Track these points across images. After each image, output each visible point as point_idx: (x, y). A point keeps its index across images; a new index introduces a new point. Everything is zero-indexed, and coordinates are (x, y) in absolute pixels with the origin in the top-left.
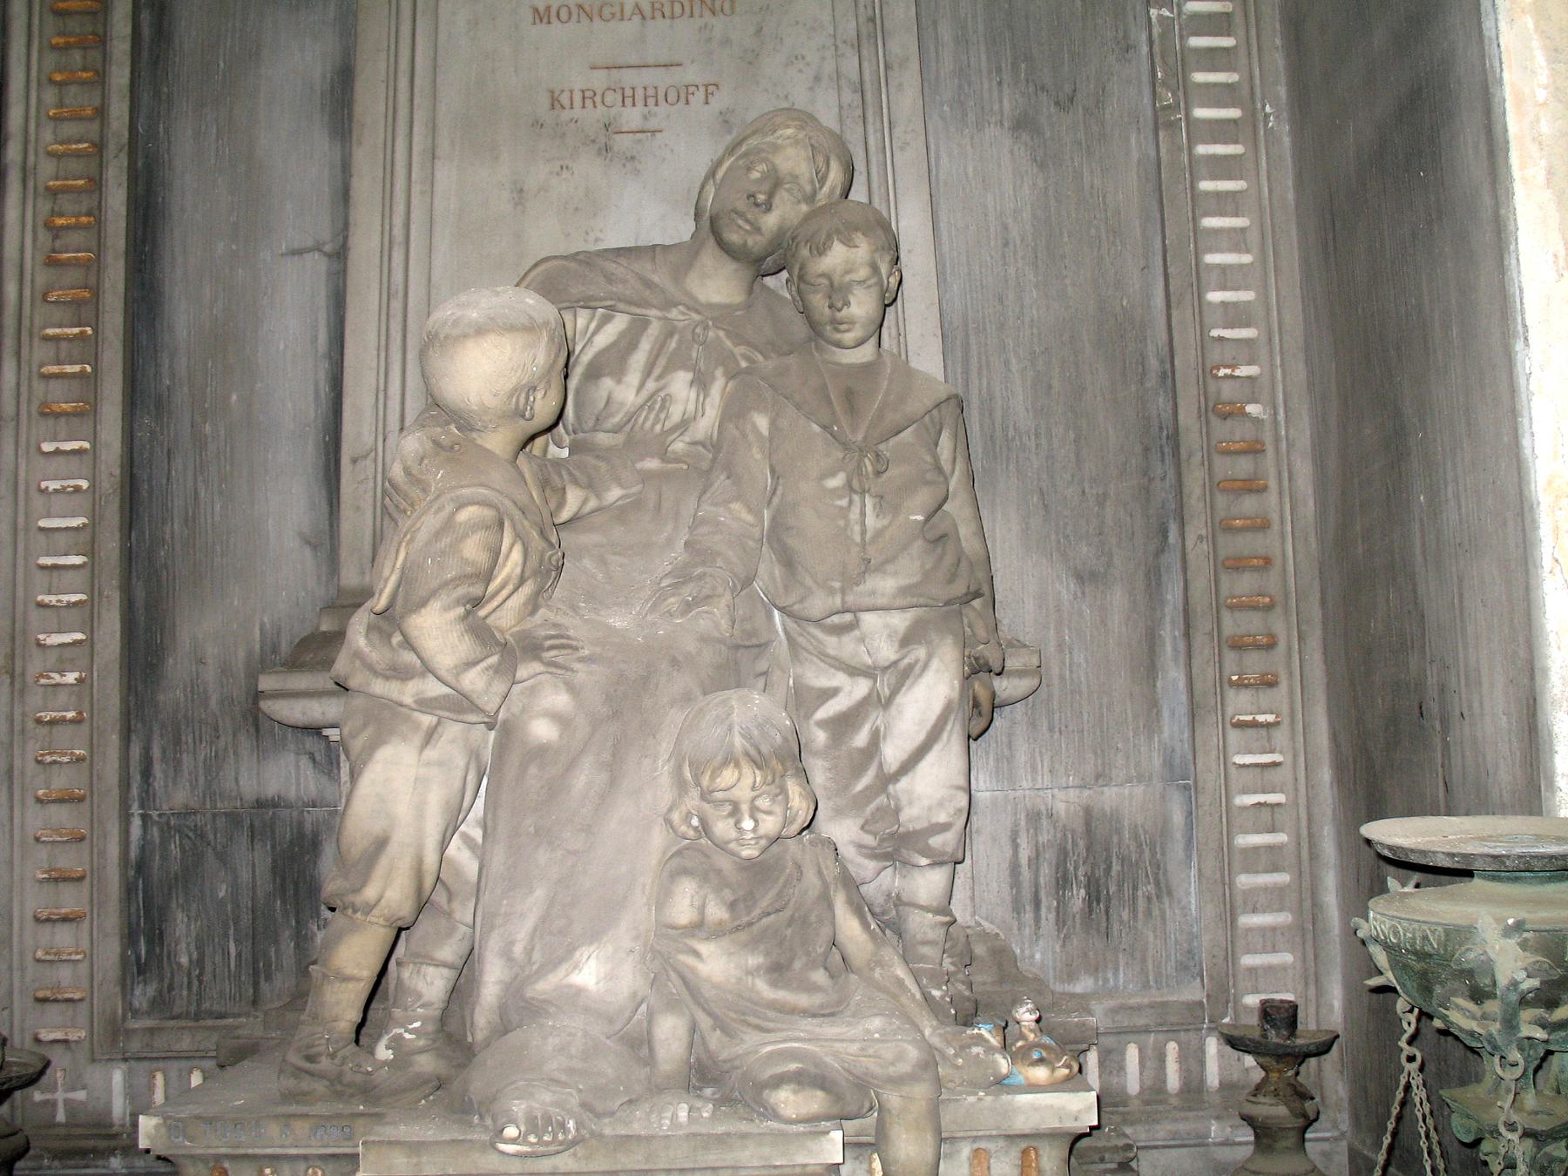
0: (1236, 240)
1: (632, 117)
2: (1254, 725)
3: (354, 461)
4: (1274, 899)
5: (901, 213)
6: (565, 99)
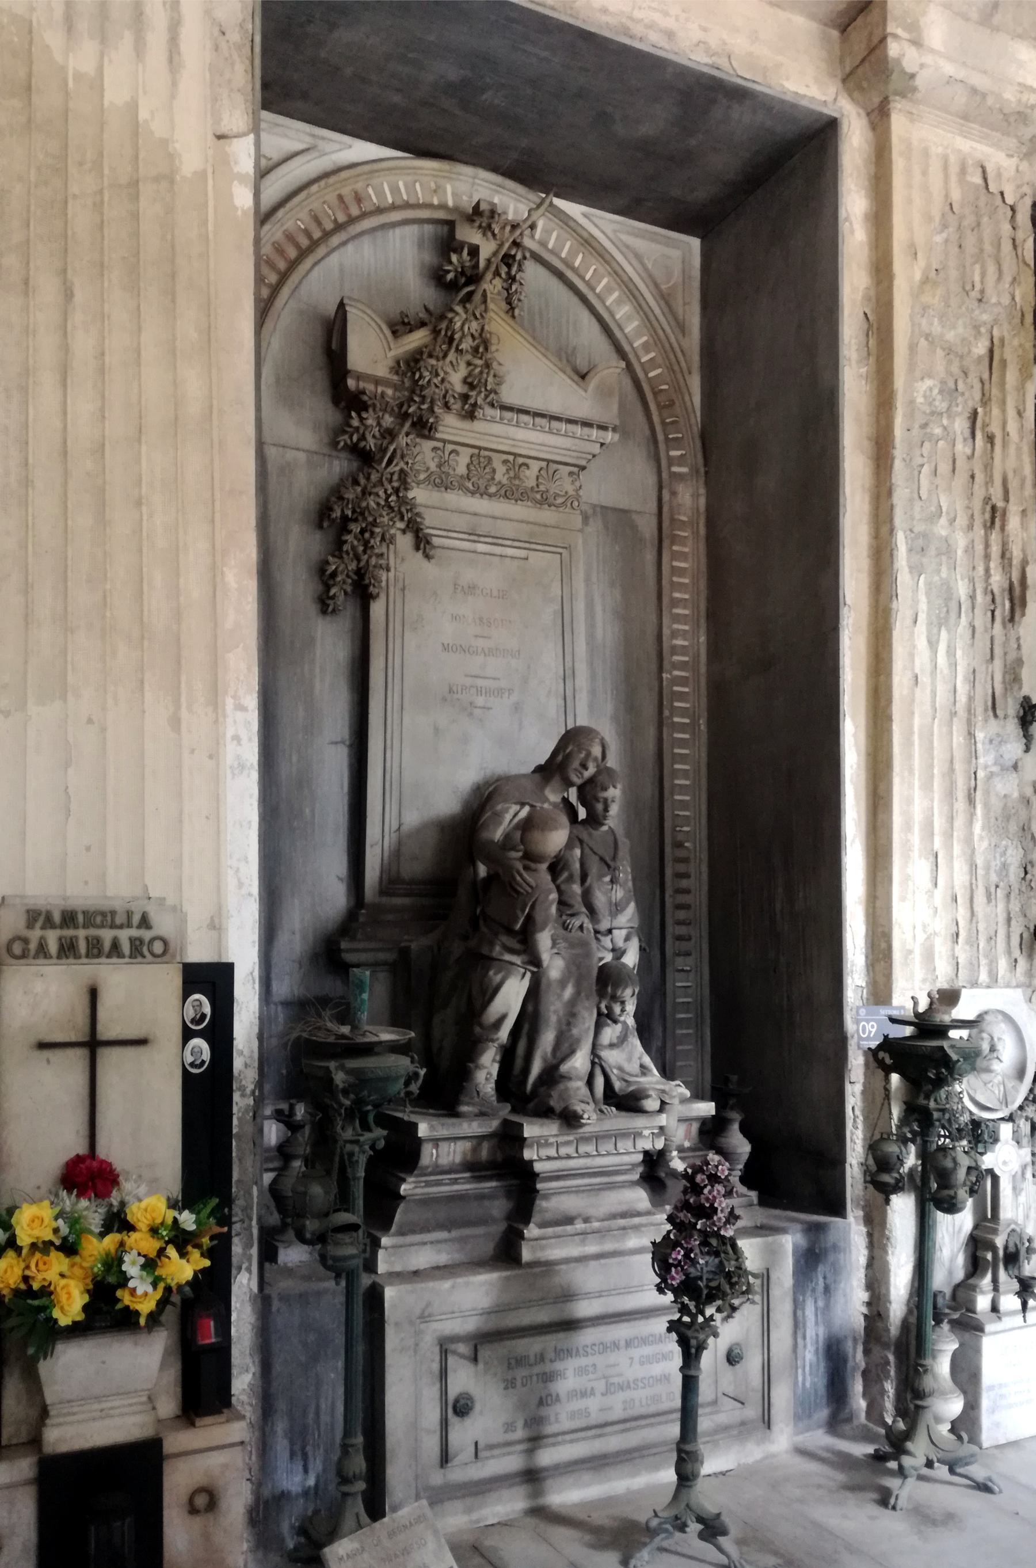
0: (685, 774)
1: (480, 701)
2: (683, 970)
3: (372, 846)
4: (675, 603)
5: (760, 1394)
6: (455, 689)
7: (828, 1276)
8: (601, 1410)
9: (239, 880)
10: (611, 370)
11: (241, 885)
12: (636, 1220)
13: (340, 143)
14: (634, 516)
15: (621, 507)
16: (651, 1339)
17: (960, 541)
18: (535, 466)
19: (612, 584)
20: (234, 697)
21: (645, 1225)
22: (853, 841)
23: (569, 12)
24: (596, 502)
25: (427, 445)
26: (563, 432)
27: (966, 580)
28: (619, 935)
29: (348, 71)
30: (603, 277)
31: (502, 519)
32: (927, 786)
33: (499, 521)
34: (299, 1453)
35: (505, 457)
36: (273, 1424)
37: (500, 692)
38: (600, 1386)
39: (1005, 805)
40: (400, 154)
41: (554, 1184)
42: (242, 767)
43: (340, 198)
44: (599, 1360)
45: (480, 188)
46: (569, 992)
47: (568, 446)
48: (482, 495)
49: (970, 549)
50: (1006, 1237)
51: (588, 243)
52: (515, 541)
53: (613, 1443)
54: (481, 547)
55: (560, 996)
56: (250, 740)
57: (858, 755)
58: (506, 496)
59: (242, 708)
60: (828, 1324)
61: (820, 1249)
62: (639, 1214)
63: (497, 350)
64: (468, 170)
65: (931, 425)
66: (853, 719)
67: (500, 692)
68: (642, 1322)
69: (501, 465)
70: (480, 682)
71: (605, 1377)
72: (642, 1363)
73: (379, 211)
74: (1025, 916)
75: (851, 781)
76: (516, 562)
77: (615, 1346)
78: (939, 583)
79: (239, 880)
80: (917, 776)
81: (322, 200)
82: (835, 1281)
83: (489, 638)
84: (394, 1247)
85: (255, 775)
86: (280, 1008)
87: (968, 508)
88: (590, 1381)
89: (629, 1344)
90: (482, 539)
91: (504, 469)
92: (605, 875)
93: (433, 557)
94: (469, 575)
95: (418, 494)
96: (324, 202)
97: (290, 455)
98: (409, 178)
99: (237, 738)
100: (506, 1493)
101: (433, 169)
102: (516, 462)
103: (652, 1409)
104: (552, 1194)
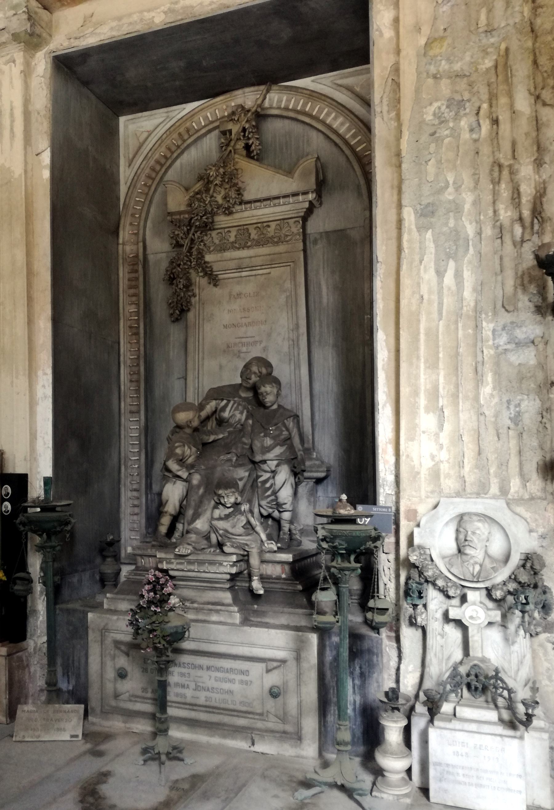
1: (244, 349)
7: (364, 667)
8: (192, 697)
9: (44, 442)
10: (309, 161)
11: (45, 444)
12: (219, 607)
13: (178, 109)
14: (348, 231)
15: (339, 229)
16: (222, 669)
17: (468, 198)
18: (273, 225)
19: (333, 272)
20: (43, 370)
21: (224, 611)
22: (384, 406)
23: (190, 16)
24: (321, 231)
25: (214, 233)
26: (244, 209)
27: (474, 224)
28: (272, 464)
29: (149, 84)
30: (325, 109)
31: (255, 257)
32: (433, 365)
33: (253, 259)
34: (66, 674)
35: (255, 226)
36: (401, 721)
37: (255, 343)
38: (192, 685)
39: (519, 371)
40: (209, 100)
41: (181, 583)
42: (46, 397)
43: (180, 134)
44: (193, 672)
45: (249, 97)
46: (201, 491)
47: (289, 209)
48: (243, 248)
49: (476, 203)
50: (469, 668)
51: (313, 95)
52: (262, 266)
53: (203, 716)
54: (244, 274)
55: (197, 493)
56: (49, 386)
57: (389, 352)
58: (256, 245)
59: (45, 374)
60: (364, 696)
61: (357, 649)
62: (223, 605)
63: (241, 176)
64: (239, 92)
65: (439, 131)
66: (385, 331)
67: (255, 343)
68: (216, 659)
69: (253, 230)
70: (244, 340)
71: (195, 681)
72: (216, 680)
73: (197, 131)
74: (542, 449)
75: (383, 369)
76: (264, 277)
77: (201, 667)
78: (448, 231)
79: (44, 442)
80: (422, 360)
81: (171, 139)
82: (369, 672)
83: (249, 317)
84: (112, 598)
85: (50, 400)
86: (156, 496)
87: (474, 174)
88: (186, 681)
89: (208, 668)
90: (244, 270)
91: (255, 232)
92: (261, 433)
93: (218, 285)
94: (237, 289)
95: (208, 258)
96: (173, 139)
97: (159, 256)
98: (212, 110)
99: (44, 386)
100: (143, 721)
101: (221, 100)
102: (261, 226)
103: (222, 706)
104: (181, 587)
